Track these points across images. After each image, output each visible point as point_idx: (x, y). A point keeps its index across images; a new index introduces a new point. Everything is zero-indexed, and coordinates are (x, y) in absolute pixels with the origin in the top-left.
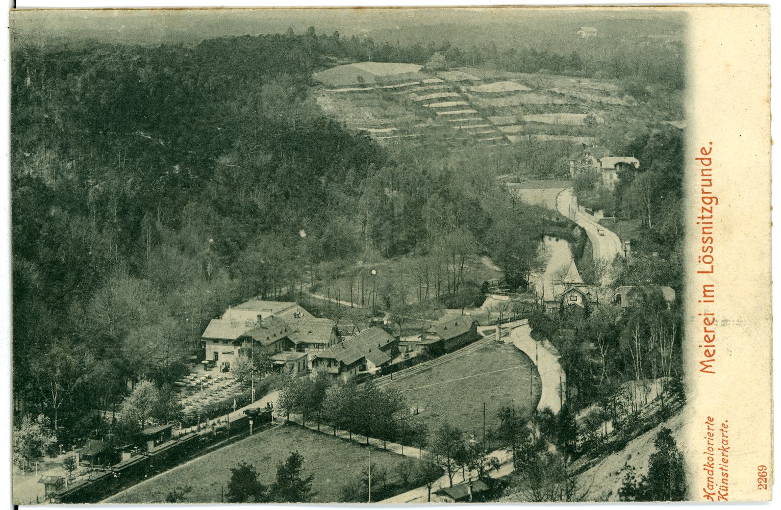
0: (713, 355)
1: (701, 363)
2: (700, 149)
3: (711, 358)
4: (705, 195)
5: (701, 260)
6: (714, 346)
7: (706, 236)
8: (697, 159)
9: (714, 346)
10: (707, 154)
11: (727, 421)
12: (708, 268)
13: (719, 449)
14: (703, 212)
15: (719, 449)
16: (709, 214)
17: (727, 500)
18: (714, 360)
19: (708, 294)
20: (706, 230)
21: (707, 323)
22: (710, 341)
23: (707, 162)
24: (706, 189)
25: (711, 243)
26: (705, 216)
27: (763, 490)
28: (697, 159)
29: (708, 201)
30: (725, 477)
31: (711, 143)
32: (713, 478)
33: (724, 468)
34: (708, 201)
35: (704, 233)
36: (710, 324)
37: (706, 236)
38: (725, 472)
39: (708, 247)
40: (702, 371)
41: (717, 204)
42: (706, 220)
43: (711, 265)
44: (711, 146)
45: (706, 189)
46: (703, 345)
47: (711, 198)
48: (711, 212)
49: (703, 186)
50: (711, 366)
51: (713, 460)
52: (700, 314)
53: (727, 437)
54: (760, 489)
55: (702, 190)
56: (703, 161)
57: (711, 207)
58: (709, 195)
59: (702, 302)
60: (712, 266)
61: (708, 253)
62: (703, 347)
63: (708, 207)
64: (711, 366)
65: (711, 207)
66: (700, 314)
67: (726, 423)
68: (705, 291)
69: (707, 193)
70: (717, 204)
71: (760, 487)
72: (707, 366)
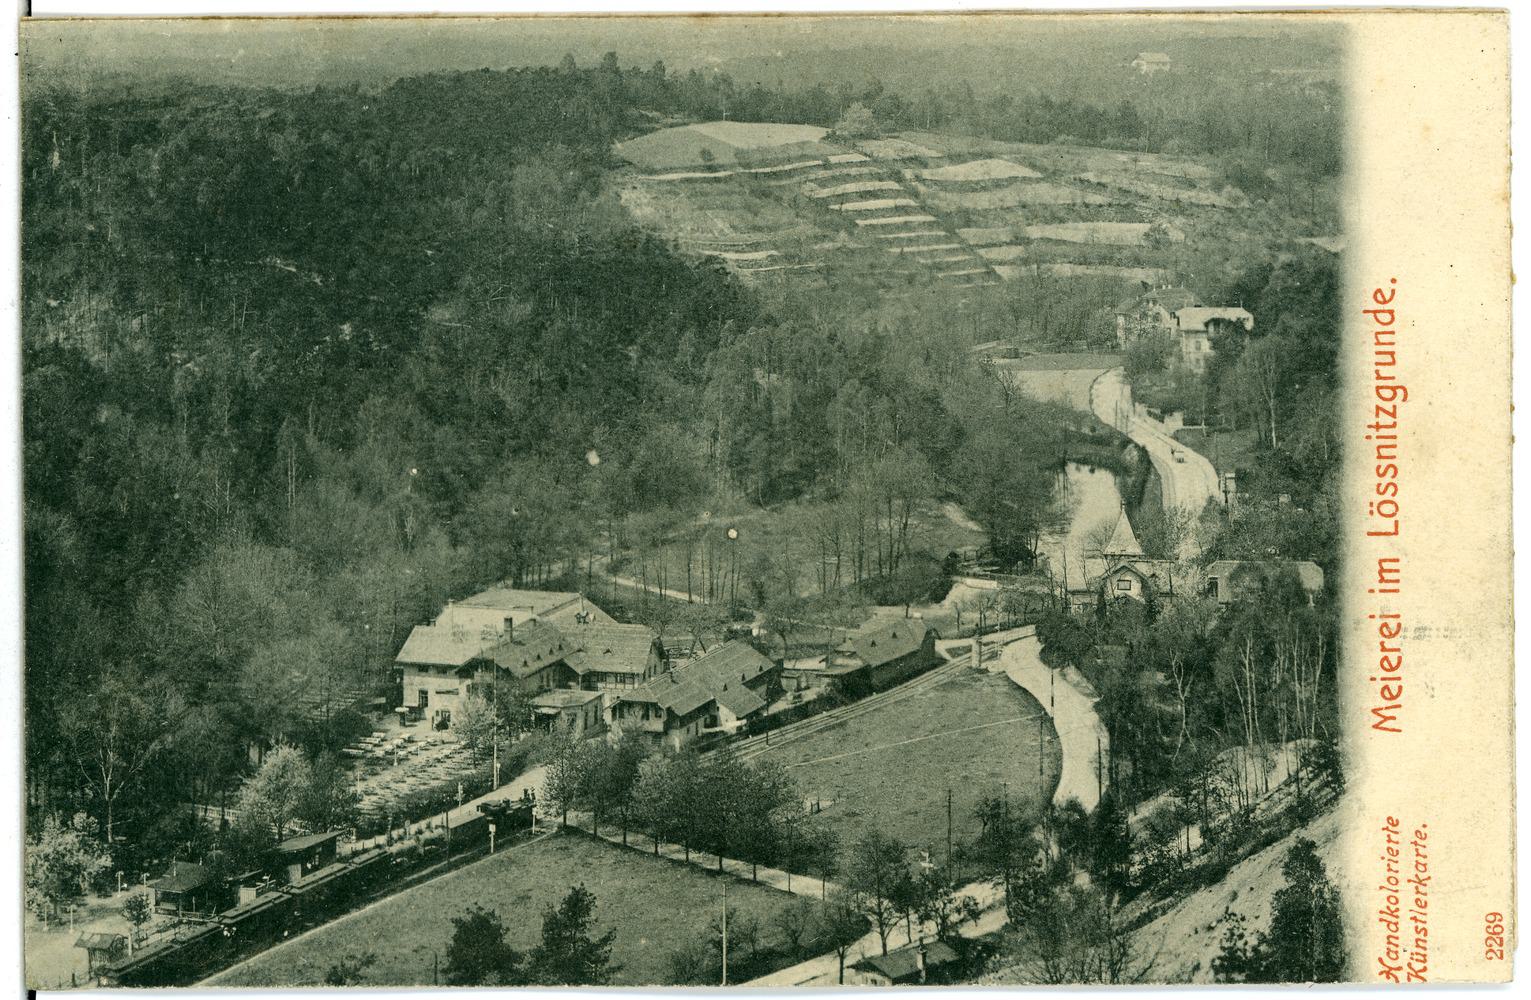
0: (1398, 696)
1: (1375, 711)
2: (1372, 293)
3: (1393, 703)
4: (1382, 383)
5: (1375, 509)
6: (1399, 679)
7: (1384, 463)
8: (1366, 312)
9: (1399, 679)
10: (1385, 302)
11: (1425, 826)
12: (1387, 525)
13: (1409, 881)
14: (1377, 415)
15: (1409, 881)
16: (1389, 420)
17: (1424, 980)
18: (1399, 706)
19: (1387, 576)
20: (1384, 452)
21: (1387, 633)
22: (1392, 669)
23: (1386, 318)
24: (1385, 371)
25: (1393, 477)
26: (1381, 424)
27: (1496, 960)
28: (1366, 312)
29: (1387, 393)
30: (1421, 936)
31: (1394, 281)
32: (1397, 938)
33: (1419, 917)
34: (1387, 393)
35: (1380, 457)
36: (1392, 635)
37: (1384, 463)
38: (1420, 926)
39: (1389, 485)
40: (1376, 726)
41: (1405, 400)
42: (1383, 432)
43: (1393, 519)
44: (1393, 286)
45: (1385, 371)
46: (1378, 677)
47: (1394, 389)
48: (1393, 415)
49: (1377, 364)
50: (1393, 718)
51: (1397, 902)
52: (1372, 617)
53: (1425, 857)
54: (1491, 958)
55: (1377, 372)
56: (1379, 315)
57: (1395, 407)
58: (1390, 383)
59: (1377, 591)
60: (1396, 522)
61: (1387, 496)
62: (1378, 680)
63: (1388, 406)
64: (1393, 718)
65: (1395, 407)
66: (1372, 617)
67: (1423, 830)
68: (1382, 571)
69: (1385, 378)
70: (1405, 400)
71: (1490, 955)
72: (1386, 719)
